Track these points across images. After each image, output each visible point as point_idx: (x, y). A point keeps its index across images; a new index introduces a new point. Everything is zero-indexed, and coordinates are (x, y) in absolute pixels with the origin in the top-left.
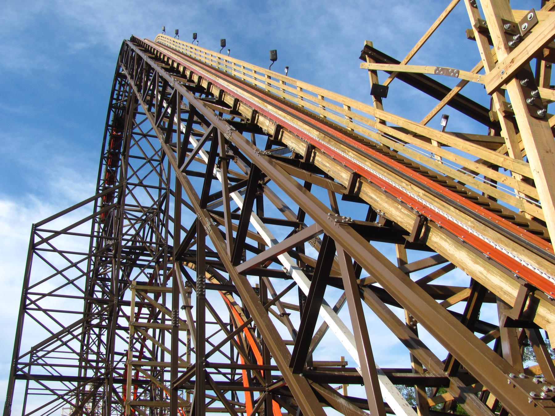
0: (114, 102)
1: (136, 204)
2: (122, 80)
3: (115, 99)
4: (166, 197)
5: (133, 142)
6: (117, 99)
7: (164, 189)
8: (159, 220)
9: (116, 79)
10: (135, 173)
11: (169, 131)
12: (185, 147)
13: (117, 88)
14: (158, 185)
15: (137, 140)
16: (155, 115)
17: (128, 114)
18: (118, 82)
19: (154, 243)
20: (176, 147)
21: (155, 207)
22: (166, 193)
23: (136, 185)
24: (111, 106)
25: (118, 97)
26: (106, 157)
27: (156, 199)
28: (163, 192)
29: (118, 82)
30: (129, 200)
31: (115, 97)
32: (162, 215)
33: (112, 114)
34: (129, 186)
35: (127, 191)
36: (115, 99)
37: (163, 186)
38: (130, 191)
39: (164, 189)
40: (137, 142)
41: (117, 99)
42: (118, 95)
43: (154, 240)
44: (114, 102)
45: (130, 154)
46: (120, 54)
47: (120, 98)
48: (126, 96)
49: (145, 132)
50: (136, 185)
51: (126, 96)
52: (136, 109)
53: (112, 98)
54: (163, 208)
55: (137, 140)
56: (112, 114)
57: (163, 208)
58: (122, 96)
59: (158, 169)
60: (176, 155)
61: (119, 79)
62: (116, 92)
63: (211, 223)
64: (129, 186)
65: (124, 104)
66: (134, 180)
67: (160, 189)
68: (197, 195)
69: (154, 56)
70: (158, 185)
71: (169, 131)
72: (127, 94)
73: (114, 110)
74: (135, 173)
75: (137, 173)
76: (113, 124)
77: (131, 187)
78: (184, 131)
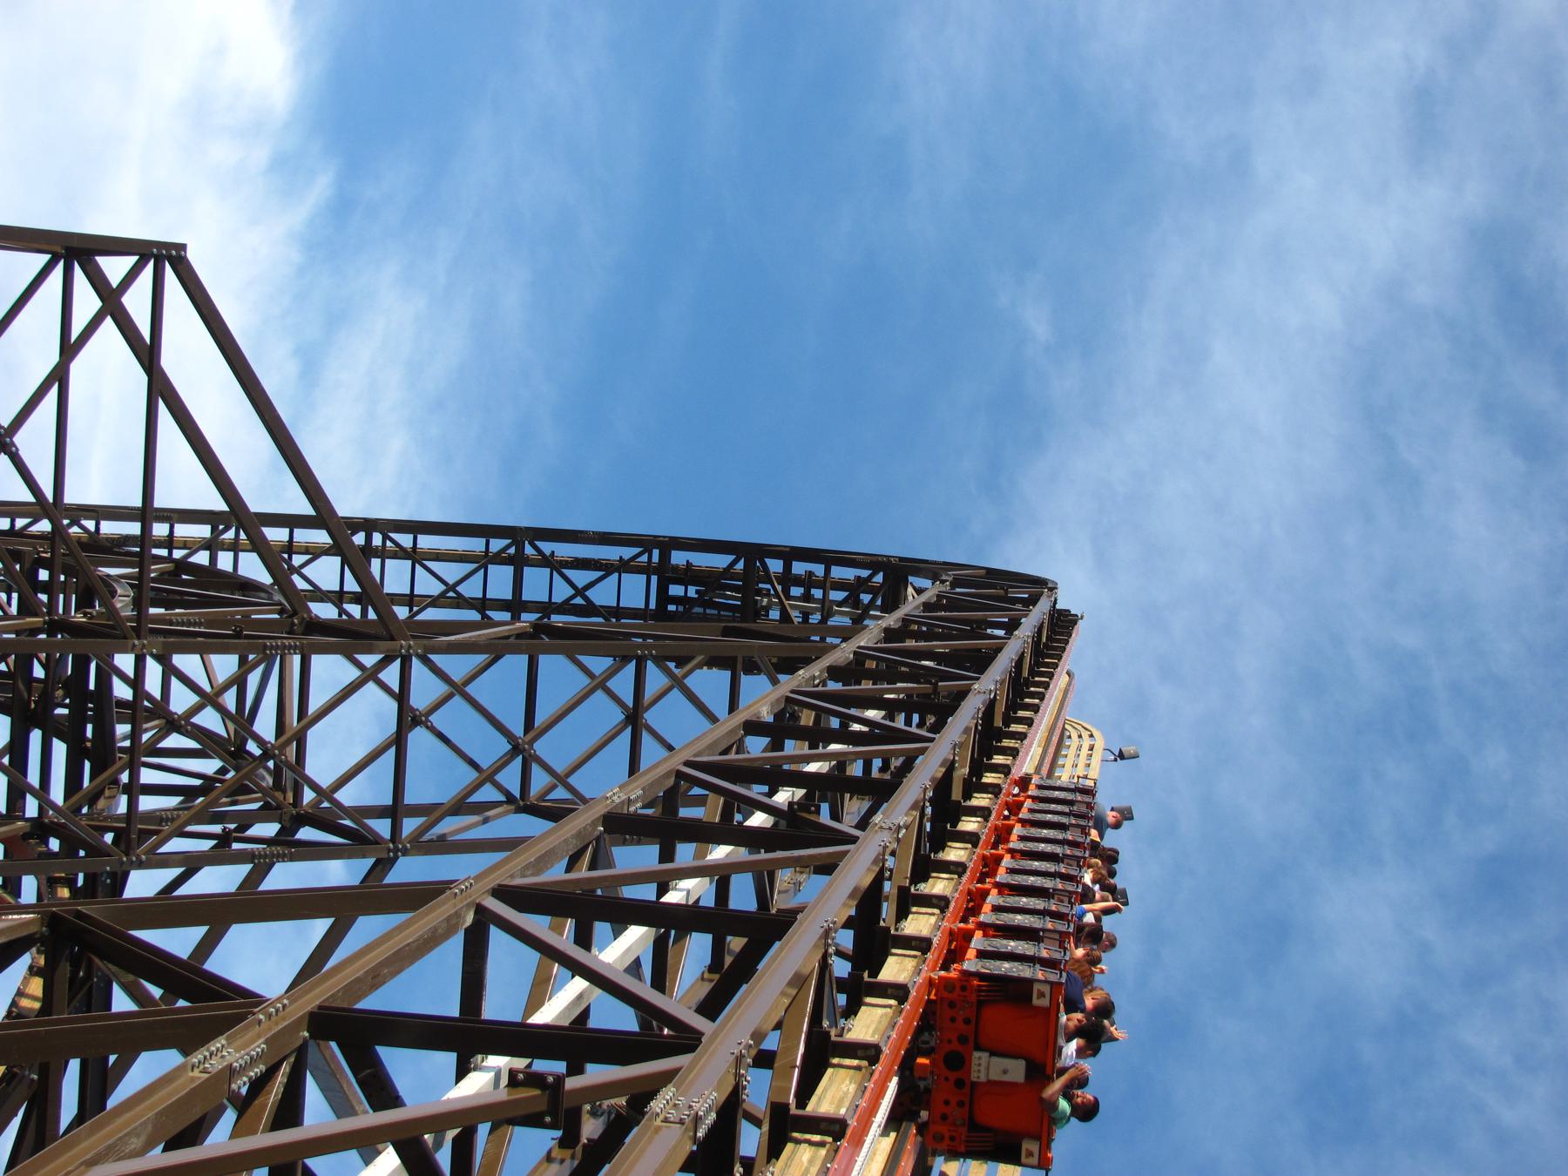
0: (775, 566)
1: (314, 705)
2: (874, 591)
3: (787, 567)
4: (359, 841)
5: (598, 664)
6: (787, 579)
7: (396, 829)
8: (246, 820)
9: (874, 563)
10: (458, 689)
11: (662, 826)
12: (595, 909)
13: (838, 572)
14: (410, 798)
15: (610, 684)
16: (732, 756)
17: (727, 632)
18: (865, 573)
19: (132, 804)
20: (592, 867)
21: (309, 795)
22: (376, 840)
23: (402, 697)
24: (754, 553)
25: (798, 581)
26: (520, 549)
27: (346, 796)
28: (382, 827)
29: (865, 573)
30: (330, 671)
31: (799, 568)
32: (269, 829)
33: (720, 561)
34: (396, 666)
35: (369, 660)
36: (787, 567)
37: (410, 825)
38: (371, 675)
39: (396, 829)
40: (600, 684)
41: (787, 579)
42: (808, 582)
43: (147, 803)
44: (775, 566)
45: (545, 661)
46: (991, 572)
47: (796, 591)
48: (806, 615)
49: (650, 717)
50: (402, 697)
51: (806, 615)
52: (752, 668)
53: (791, 554)
54: (306, 833)
55: (610, 684)
56: (720, 561)
57: (306, 833)
58: (807, 597)
59: (488, 793)
60: (556, 873)
61: (879, 578)
62: (819, 569)
63: (243, 1070)
64: (396, 666)
65: (767, 609)
66: (425, 688)
67: (395, 811)
68: (375, 986)
69: (998, 722)
70: (410, 798)
71: (662, 826)
72: (815, 618)
73: (740, 565)
74: (458, 689)
75: (457, 699)
76: (676, 568)
77: (391, 675)
78: (672, 897)
